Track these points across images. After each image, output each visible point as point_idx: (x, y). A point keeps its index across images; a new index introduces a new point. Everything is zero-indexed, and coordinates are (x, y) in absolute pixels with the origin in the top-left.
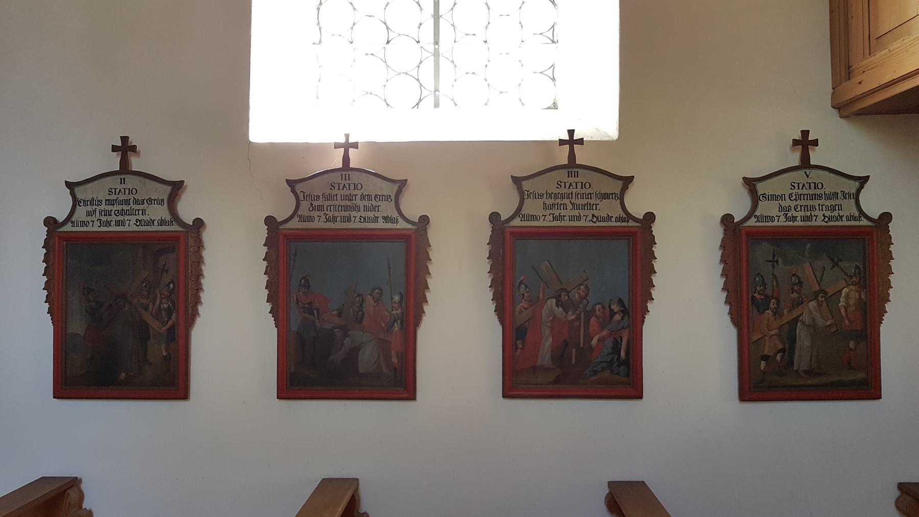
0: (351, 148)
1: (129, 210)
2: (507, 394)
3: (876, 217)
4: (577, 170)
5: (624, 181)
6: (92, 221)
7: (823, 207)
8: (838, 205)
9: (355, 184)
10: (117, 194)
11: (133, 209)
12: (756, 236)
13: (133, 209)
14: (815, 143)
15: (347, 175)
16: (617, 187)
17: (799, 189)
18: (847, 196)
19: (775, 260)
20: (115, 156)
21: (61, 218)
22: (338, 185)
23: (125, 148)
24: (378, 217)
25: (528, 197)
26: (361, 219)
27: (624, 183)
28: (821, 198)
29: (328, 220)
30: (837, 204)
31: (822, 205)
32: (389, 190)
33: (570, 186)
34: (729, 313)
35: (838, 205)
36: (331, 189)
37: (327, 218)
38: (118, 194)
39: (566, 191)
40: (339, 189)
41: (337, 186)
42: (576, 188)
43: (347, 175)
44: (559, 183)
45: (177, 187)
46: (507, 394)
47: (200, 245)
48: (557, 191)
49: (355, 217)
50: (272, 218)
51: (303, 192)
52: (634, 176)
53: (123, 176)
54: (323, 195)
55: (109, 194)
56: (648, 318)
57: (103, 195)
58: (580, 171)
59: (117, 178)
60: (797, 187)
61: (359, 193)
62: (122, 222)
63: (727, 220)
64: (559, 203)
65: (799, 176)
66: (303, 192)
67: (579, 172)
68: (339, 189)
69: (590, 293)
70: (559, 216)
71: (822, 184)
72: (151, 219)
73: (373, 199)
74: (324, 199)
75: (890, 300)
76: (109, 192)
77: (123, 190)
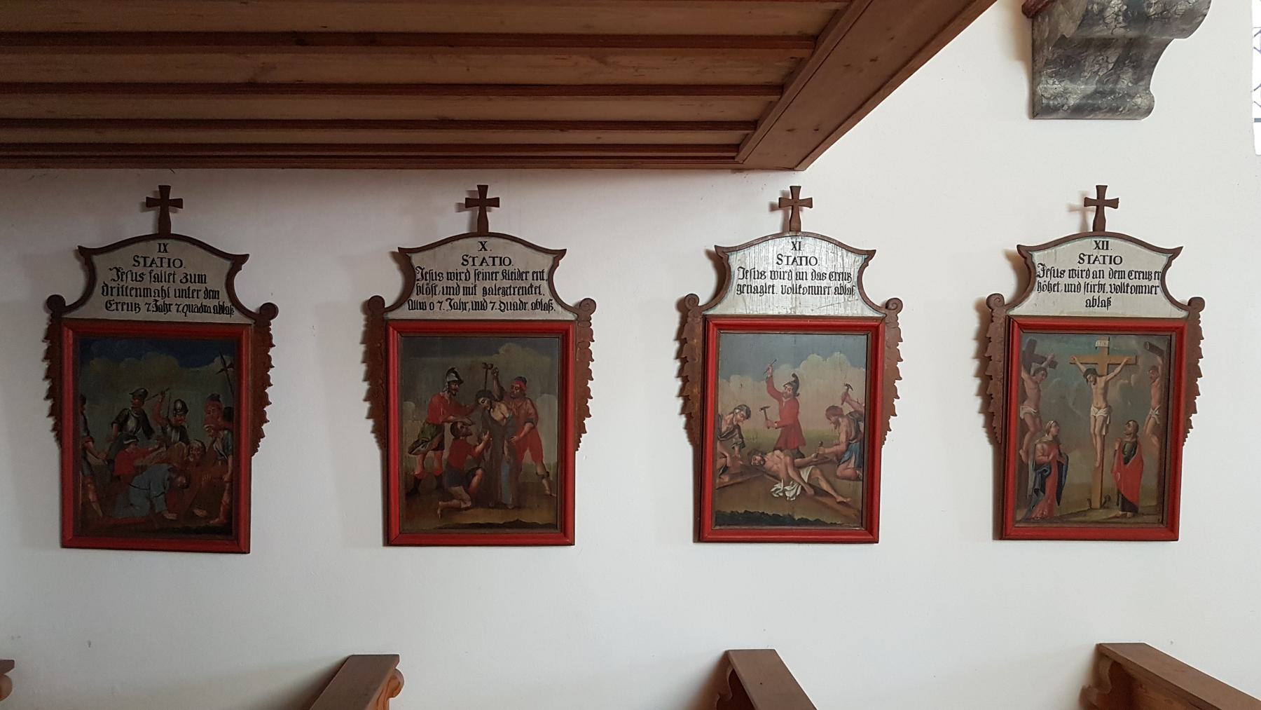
0: (1106, 206)
1: (185, 290)
2: (1004, 530)
3: (879, 302)
4: (1107, 240)
5: (555, 256)
6: (439, 302)
7: (114, 290)
8: (136, 289)
9: (1111, 257)
10: (1091, 262)
11: (1088, 284)
12: (410, 329)
13: (1088, 284)
14: (1114, 204)
15: (1105, 243)
16: (547, 261)
17: (1089, 263)
18: (428, 275)
19: (227, 365)
20: (490, 213)
21: (69, 302)
22: (786, 258)
23: (1100, 202)
24: (170, 305)
25: (119, 278)
26: (501, 307)
27: (554, 258)
28: (763, 277)
29: (158, 309)
30: (196, 289)
31: (514, 288)
32: (545, 262)
33: (482, 262)
34: (263, 436)
35: (136, 289)
36: (1079, 262)
37: (452, 304)
38: (1094, 263)
39: (1093, 268)
40: (788, 264)
41: (785, 259)
42: (162, 266)
43: (1105, 243)
44: (1082, 256)
45: (238, 261)
46: (1004, 530)
47: (266, 342)
48: (1081, 267)
49: (441, 303)
50: (589, 301)
51: (742, 268)
52: (875, 251)
53: (162, 241)
54: (150, 273)
55: (463, 264)
56: (889, 435)
57: (455, 265)
58: (1111, 241)
59: (154, 244)
60: (1086, 261)
61: (809, 269)
62: (482, 305)
63: (374, 307)
64: (130, 287)
65: (1088, 245)
66: (742, 268)
67: (1109, 243)
68: (788, 264)
69: (87, 417)
70: (1093, 299)
71: (181, 261)
72: (521, 302)
73: (1126, 275)
74: (153, 279)
75: (268, 419)
76: (462, 261)
77: (1101, 259)
